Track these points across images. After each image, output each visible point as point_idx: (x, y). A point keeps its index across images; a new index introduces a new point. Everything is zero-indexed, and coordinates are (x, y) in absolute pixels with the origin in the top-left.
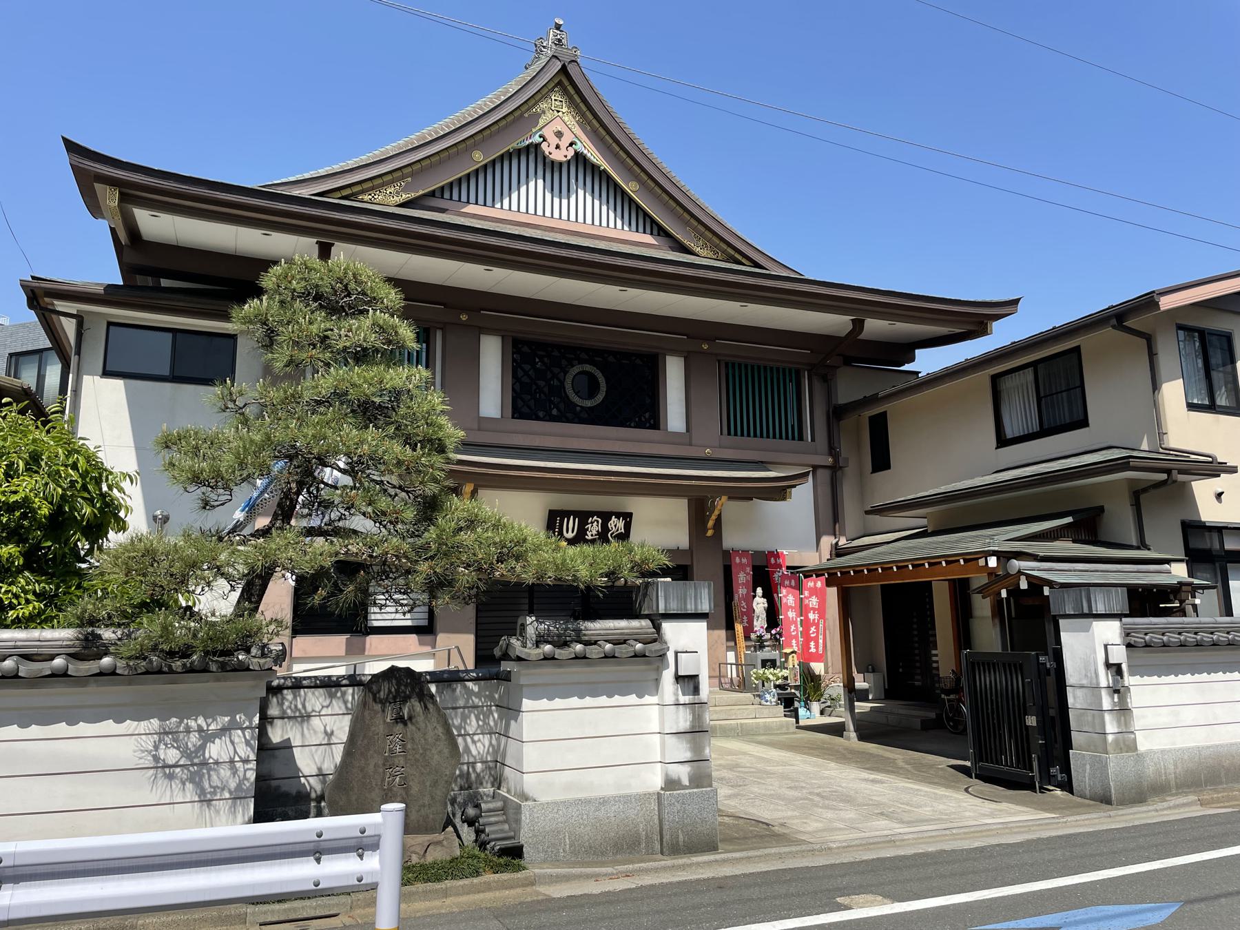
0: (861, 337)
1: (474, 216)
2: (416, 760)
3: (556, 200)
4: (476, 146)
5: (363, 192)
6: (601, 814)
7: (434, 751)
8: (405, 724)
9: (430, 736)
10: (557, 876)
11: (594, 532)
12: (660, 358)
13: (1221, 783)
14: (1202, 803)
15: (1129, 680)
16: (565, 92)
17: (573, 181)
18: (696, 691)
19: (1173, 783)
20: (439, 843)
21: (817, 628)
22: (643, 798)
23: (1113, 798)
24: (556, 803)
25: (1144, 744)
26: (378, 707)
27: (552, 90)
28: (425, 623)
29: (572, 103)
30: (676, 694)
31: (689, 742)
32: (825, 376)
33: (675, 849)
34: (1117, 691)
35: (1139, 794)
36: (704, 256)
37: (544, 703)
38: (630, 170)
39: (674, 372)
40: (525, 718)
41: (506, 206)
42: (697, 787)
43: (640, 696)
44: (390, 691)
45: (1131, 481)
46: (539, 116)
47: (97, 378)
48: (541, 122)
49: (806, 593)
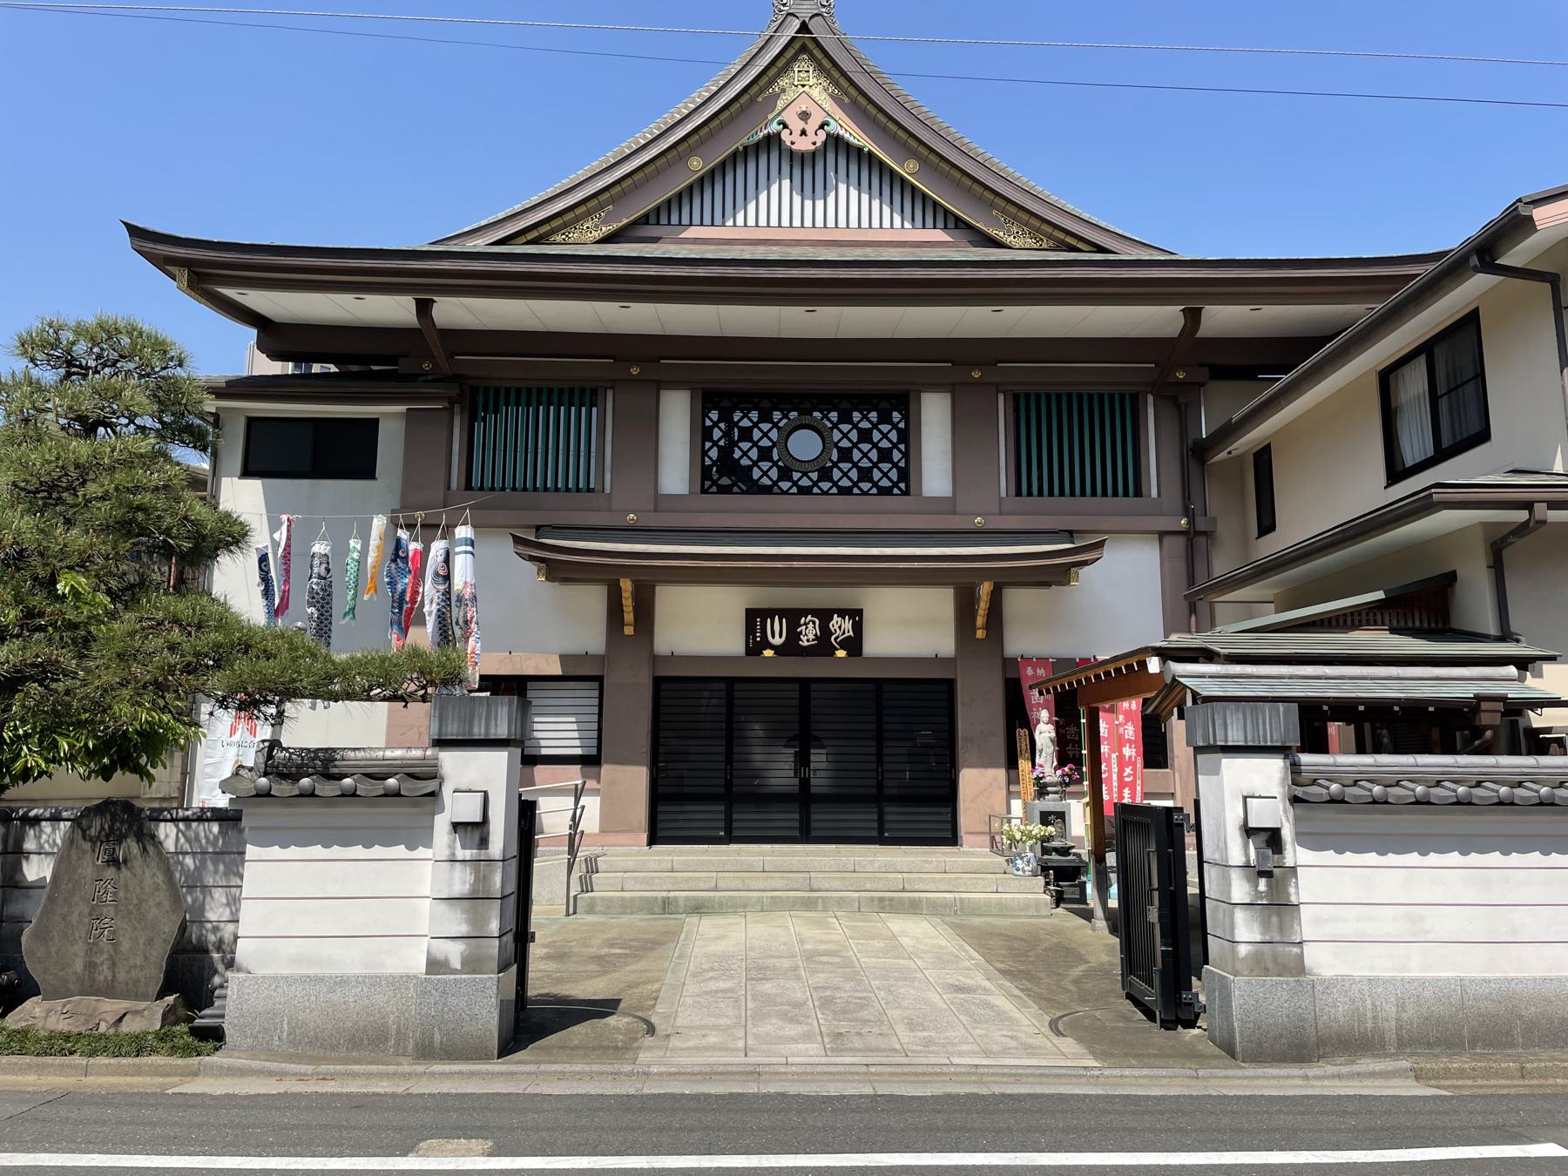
0: (1200, 334)
1: (696, 241)
2: (130, 912)
3: (808, 203)
4: (692, 151)
5: (554, 232)
6: (336, 997)
7: (151, 903)
8: (119, 869)
9: (148, 881)
10: (229, 1069)
11: (811, 637)
12: (912, 399)
13: (1512, 1045)
14: (1419, 1076)
15: (1295, 853)
16: (813, 58)
17: (831, 174)
18: (484, 843)
19: (1391, 1036)
20: (136, 1012)
21: (1134, 769)
22: (399, 982)
23: (1238, 1049)
24: (275, 978)
25: (1322, 961)
26: (87, 846)
27: (795, 58)
28: (594, 751)
29: (821, 68)
30: (452, 847)
31: (464, 911)
32: (1180, 403)
33: (426, 1052)
34: (1268, 874)
35: (1299, 1046)
36: (1020, 246)
37: (275, 852)
38: (905, 145)
39: (935, 413)
40: (249, 870)
41: (740, 221)
42: (474, 972)
43: (411, 848)
44: (102, 828)
45: (1487, 526)
46: (777, 96)
47: (235, 479)
48: (780, 104)
49: (1121, 718)
